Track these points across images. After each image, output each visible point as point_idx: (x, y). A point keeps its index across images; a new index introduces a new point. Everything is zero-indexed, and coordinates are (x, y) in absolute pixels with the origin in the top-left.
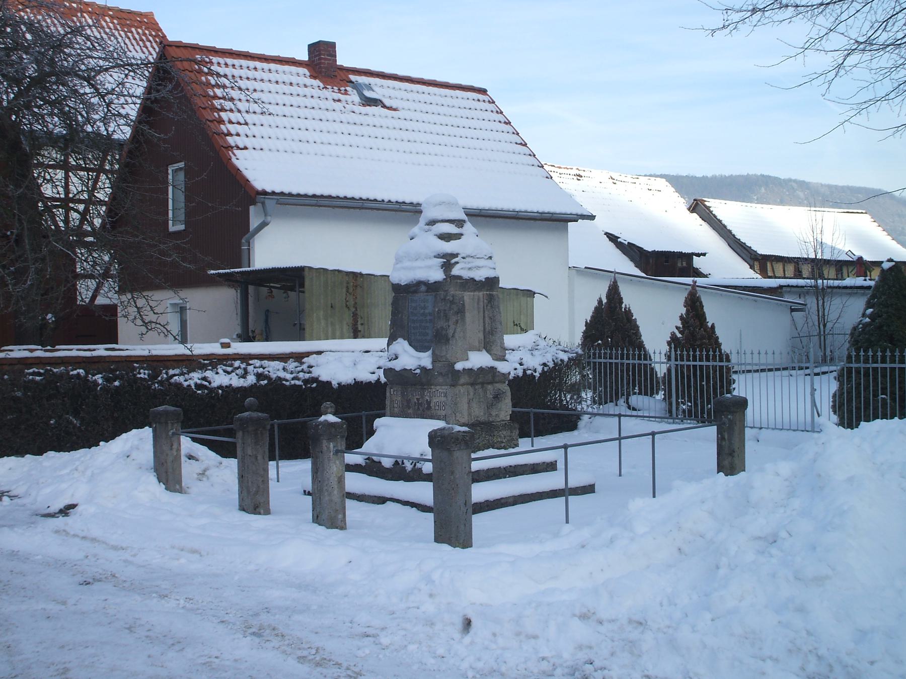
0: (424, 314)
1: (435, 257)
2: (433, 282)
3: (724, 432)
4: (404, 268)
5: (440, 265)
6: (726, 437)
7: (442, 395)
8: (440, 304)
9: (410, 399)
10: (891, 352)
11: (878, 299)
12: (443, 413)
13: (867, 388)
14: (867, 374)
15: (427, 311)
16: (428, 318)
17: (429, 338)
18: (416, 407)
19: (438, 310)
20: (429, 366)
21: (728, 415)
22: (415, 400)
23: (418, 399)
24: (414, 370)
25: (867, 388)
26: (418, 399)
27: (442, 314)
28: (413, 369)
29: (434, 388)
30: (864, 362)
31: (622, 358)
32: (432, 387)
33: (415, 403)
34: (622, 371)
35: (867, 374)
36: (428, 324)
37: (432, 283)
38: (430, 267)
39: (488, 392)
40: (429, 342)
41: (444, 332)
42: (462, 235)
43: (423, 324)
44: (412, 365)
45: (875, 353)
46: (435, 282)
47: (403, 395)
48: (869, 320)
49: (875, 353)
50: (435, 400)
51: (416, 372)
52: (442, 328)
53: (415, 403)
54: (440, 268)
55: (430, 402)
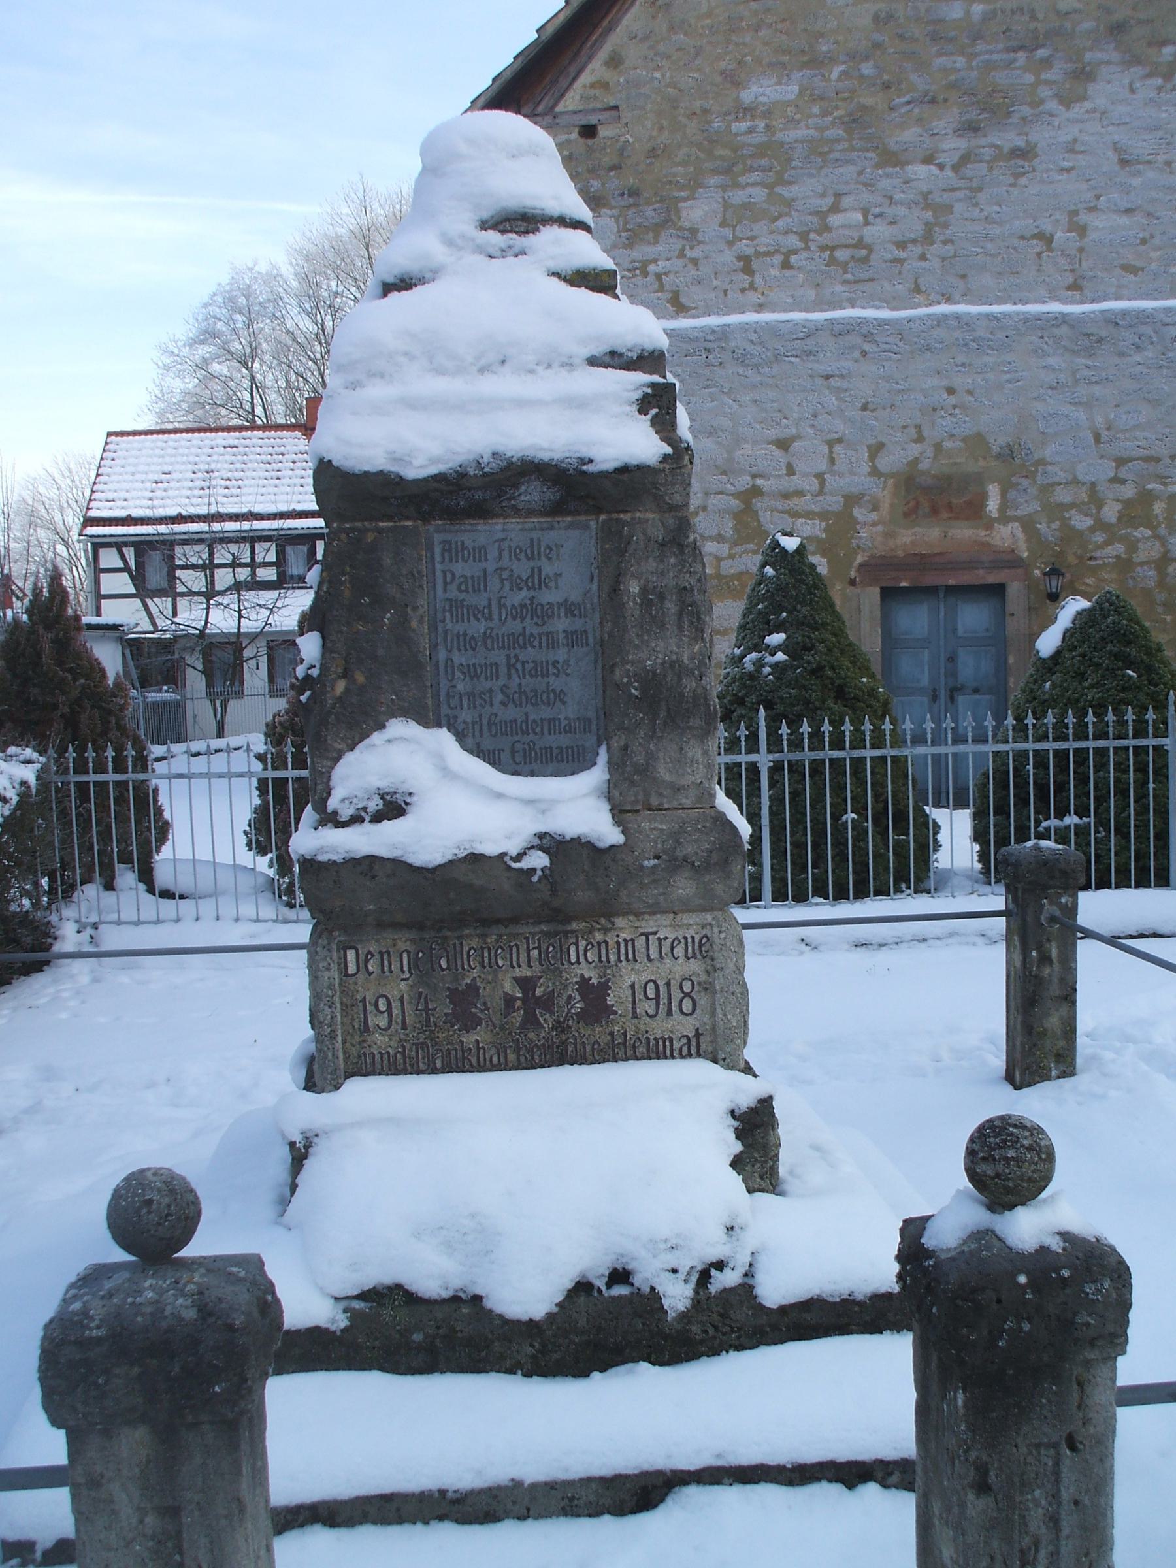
0: (531, 610)
1: (593, 362)
2: (610, 466)
3: (1049, 940)
4: (413, 404)
5: (638, 394)
6: (1054, 953)
7: (679, 951)
8: (652, 564)
9: (473, 989)
10: (115, 750)
11: (789, 612)
12: (687, 1026)
13: (818, 799)
14: (1062, 766)
15: (549, 597)
16: (561, 624)
17: (568, 711)
18: (517, 1017)
19: (644, 591)
20: (607, 833)
21: (1061, 895)
22: (508, 986)
23: (525, 984)
24: (519, 858)
25: (818, 799)
26: (525, 984)
27: (671, 607)
28: (514, 852)
29: (624, 927)
30: (116, 771)
31: (858, 763)
32: (620, 922)
33: (509, 1001)
34: (1061, 787)
35: (1062, 766)
36: (561, 654)
37: (603, 474)
38: (577, 404)
39: (709, 917)
40: (568, 730)
41: (689, 684)
42: (619, 300)
43: (530, 654)
44: (508, 837)
45: (119, 749)
46: (624, 469)
47: (422, 969)
48: (786, 657)
49: (119, 749)
50: (628, 976)
51: (524, 864)
52: (674, 665)
53: (509, 1001)
54: (635, 408)
55: (604, 987)
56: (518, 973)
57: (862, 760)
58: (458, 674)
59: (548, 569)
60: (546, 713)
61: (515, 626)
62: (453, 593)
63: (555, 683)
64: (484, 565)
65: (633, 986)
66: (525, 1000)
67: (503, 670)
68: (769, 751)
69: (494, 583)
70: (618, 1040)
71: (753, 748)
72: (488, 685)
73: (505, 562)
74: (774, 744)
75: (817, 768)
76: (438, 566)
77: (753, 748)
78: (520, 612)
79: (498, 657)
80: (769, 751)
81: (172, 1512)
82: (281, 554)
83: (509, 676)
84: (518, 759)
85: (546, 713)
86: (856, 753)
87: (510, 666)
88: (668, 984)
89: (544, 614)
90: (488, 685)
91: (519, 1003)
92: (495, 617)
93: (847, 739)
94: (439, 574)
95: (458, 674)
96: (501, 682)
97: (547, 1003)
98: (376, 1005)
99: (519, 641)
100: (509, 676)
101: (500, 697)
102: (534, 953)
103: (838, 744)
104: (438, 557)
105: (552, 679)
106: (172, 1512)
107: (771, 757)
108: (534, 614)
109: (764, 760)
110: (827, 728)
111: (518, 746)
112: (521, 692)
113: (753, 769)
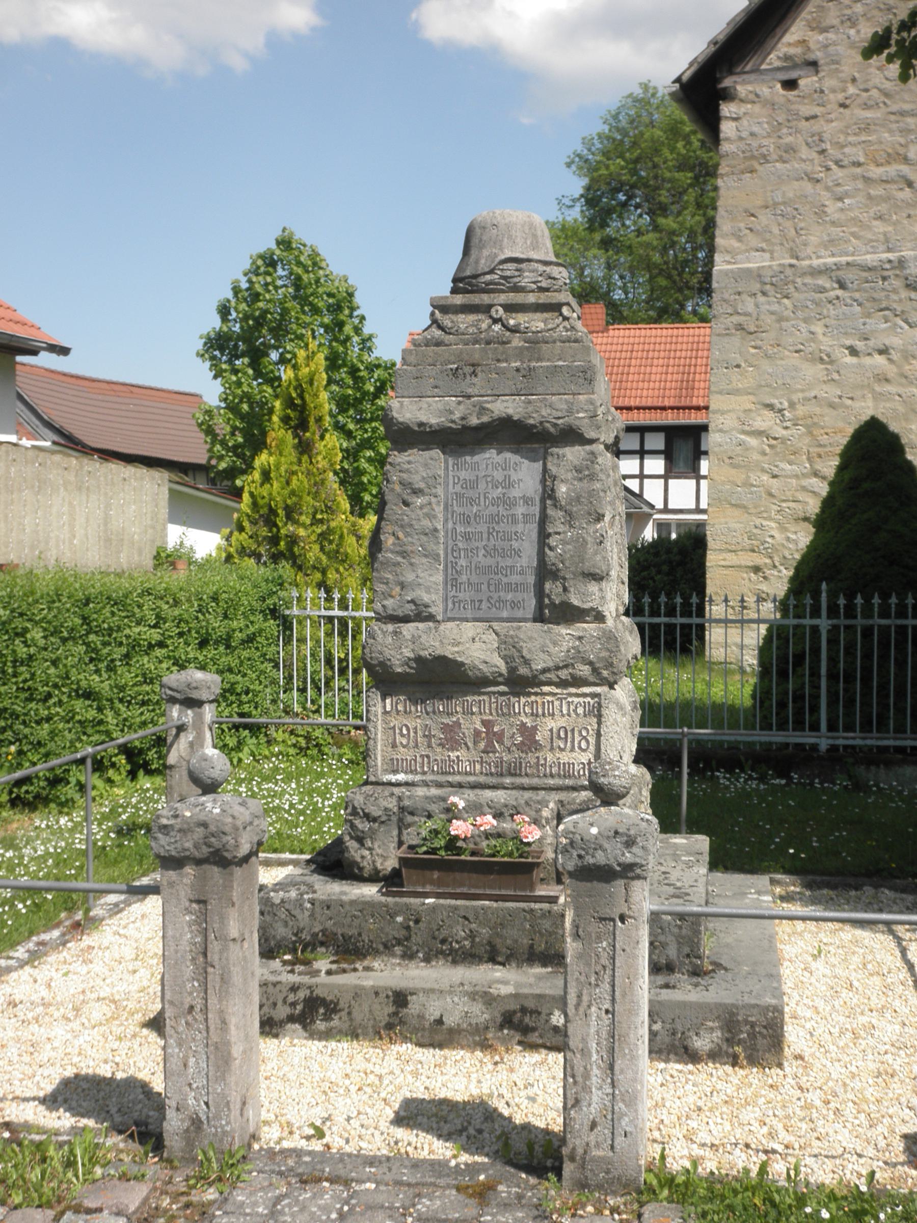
15: (516, 493)
16: (520, 510)
22: (479, 726)
33: (477, 733)
53: (477, 733)
56: (485, 718)
57: (905, 627)
58: (459, 537)
59: (514, 477)
60: (509, 562)
61: (493, 510)
62: (458, 488)
63: (515, 544)
64: (477, 473)
65: (551, 730)
66: (487, 733)
67: (485, 536)
68: (829, 617)
69: (482, 486)
70: (542, 762)
71: (816, 613)
72: (477, 544)
73: (489, 472)
74: (833, 611)
75: (867, 632)
76: (451, 473)
77: (816, 613)
78: (495, 502)
79: (483, 528)
80: (829, 617)
81: (205, 933)
82: (669, 442)
83: (489, 539)
84: (492, 588)
85: (509, 562)
86: (899, 622)
87: (489, 533)
88: (573, 730)
89: (511, 503)
90: (477, 544)
91: (484, 735)
92: (482, 503)
93: (893, 610)
94: (451, 478)
95: (459, 537)
96: (484, 543)
97: (500, 737)
98: (401, 730)
99: (495, 519)
100: (489, 539)
101: (483, 551)
102: (494, 706)
103: (884, 614)
104: (451, 468)
105: (513, 542)
106: (205, 933)
107: (830, 622)
108: (504, 503)
109: (824, 623)
110: (876, 600)
111: (492, 582)
112: (495, 549)
113: (815, 630)
